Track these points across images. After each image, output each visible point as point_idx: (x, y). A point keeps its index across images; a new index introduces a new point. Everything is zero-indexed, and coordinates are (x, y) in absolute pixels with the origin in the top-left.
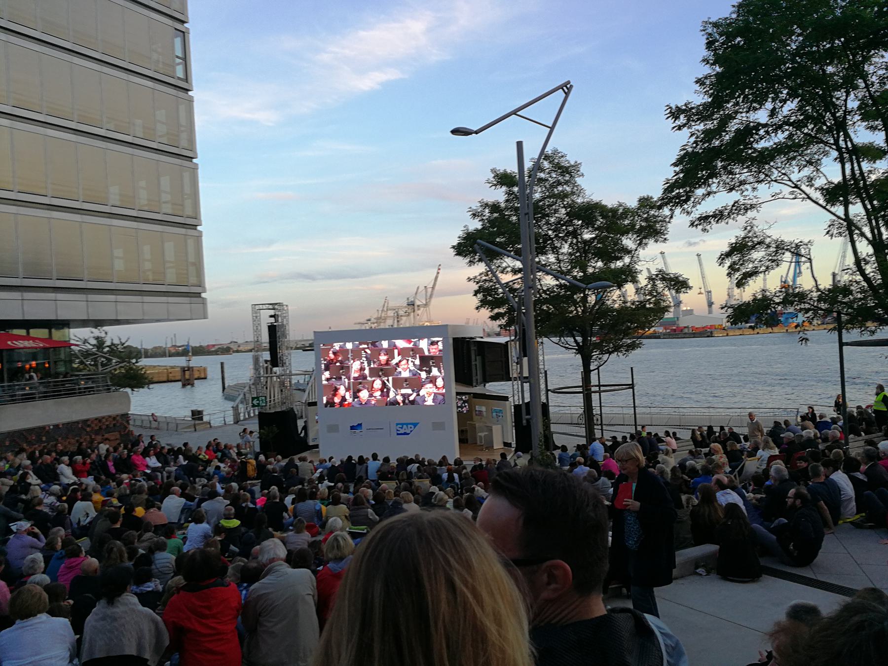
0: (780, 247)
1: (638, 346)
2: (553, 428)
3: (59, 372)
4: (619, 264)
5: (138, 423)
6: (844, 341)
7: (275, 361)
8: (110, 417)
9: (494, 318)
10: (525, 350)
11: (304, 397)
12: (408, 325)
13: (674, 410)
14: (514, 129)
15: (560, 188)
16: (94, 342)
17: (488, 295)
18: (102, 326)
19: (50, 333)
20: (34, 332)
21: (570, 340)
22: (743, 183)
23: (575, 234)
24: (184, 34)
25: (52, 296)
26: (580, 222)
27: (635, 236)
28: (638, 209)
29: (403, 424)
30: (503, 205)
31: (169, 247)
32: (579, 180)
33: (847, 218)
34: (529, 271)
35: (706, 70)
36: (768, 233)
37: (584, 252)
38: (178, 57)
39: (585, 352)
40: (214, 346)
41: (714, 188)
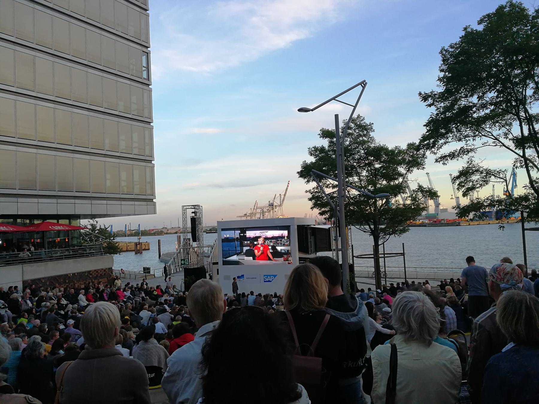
0: (489, 173)
1: (408, 230)
2: (356, 280)
3: (73, 243)
6: (525, 228)
8: (102, 269)
9: (321, 214)
10: (341, 234)
12: (269, 218)
13: (432, 269)
14: (334, 107)
17: (317, 200)
18: (95, 218)
19: (70, 222)
20: (61, 221)
21: (367, 227)
22: (467, 136)
23: (370, 164)
24: (148, 54)
25: (73, 201)
26: (372, 158)
28: (407, 150)
29: (267, 276)
30: (327, 148)
31: (136, 173)
32: (372, 134)
33: (524, 156)
34: (343, 186)
35: (442, 74)
36: (481, 165)
37: (375, 175)
39: (375, 234)
40: (153, 230)
41: (450, 139)
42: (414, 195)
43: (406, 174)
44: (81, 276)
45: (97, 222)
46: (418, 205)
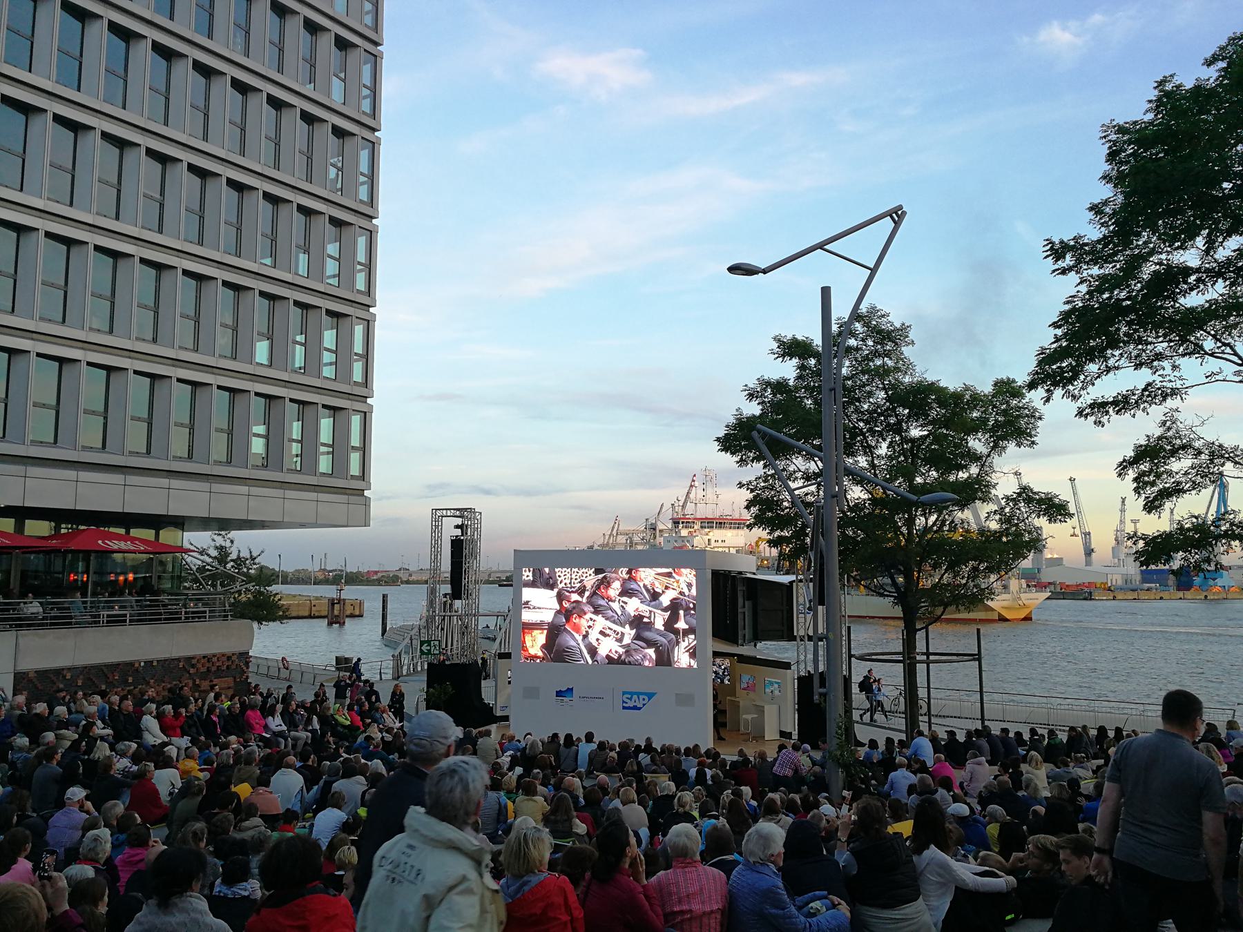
4: (963, 475)
5: (263, 670)
7: (457, 593)
9: (773, 543)
11: (494, 648)
13: (1044, 700)
14: (820, 269)
15: (879, 362)
16: (214, 553)
17: (765, 510)
20: (134, 532)
22: (1159, 357)
23: (897, 429)
25: (164, 482)
26: (907, 411)
27: (987, 436)
28: (993, 396)
29: (632, 694)
30: (791, 383)
32: (907, 351)
38: (362, 174)
40: (376, 573)
42: (1007, 510)
43: (989, 455)
44: (169, 667)
45: (232, 542)
46: (1019, 534)
